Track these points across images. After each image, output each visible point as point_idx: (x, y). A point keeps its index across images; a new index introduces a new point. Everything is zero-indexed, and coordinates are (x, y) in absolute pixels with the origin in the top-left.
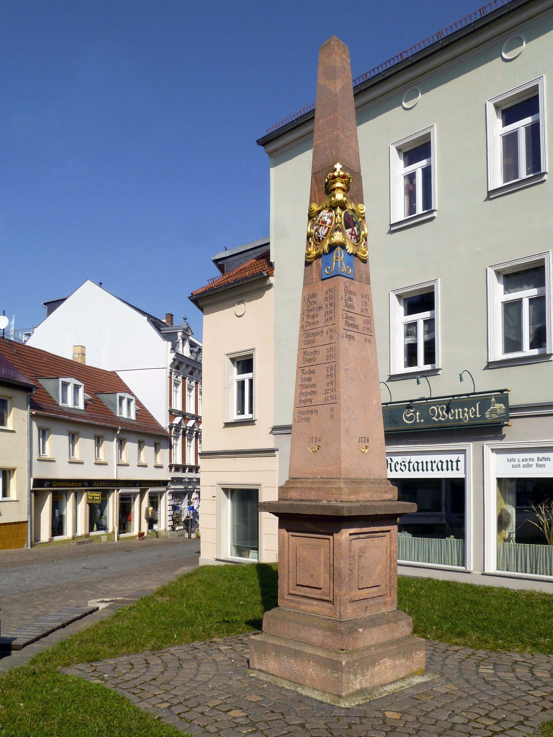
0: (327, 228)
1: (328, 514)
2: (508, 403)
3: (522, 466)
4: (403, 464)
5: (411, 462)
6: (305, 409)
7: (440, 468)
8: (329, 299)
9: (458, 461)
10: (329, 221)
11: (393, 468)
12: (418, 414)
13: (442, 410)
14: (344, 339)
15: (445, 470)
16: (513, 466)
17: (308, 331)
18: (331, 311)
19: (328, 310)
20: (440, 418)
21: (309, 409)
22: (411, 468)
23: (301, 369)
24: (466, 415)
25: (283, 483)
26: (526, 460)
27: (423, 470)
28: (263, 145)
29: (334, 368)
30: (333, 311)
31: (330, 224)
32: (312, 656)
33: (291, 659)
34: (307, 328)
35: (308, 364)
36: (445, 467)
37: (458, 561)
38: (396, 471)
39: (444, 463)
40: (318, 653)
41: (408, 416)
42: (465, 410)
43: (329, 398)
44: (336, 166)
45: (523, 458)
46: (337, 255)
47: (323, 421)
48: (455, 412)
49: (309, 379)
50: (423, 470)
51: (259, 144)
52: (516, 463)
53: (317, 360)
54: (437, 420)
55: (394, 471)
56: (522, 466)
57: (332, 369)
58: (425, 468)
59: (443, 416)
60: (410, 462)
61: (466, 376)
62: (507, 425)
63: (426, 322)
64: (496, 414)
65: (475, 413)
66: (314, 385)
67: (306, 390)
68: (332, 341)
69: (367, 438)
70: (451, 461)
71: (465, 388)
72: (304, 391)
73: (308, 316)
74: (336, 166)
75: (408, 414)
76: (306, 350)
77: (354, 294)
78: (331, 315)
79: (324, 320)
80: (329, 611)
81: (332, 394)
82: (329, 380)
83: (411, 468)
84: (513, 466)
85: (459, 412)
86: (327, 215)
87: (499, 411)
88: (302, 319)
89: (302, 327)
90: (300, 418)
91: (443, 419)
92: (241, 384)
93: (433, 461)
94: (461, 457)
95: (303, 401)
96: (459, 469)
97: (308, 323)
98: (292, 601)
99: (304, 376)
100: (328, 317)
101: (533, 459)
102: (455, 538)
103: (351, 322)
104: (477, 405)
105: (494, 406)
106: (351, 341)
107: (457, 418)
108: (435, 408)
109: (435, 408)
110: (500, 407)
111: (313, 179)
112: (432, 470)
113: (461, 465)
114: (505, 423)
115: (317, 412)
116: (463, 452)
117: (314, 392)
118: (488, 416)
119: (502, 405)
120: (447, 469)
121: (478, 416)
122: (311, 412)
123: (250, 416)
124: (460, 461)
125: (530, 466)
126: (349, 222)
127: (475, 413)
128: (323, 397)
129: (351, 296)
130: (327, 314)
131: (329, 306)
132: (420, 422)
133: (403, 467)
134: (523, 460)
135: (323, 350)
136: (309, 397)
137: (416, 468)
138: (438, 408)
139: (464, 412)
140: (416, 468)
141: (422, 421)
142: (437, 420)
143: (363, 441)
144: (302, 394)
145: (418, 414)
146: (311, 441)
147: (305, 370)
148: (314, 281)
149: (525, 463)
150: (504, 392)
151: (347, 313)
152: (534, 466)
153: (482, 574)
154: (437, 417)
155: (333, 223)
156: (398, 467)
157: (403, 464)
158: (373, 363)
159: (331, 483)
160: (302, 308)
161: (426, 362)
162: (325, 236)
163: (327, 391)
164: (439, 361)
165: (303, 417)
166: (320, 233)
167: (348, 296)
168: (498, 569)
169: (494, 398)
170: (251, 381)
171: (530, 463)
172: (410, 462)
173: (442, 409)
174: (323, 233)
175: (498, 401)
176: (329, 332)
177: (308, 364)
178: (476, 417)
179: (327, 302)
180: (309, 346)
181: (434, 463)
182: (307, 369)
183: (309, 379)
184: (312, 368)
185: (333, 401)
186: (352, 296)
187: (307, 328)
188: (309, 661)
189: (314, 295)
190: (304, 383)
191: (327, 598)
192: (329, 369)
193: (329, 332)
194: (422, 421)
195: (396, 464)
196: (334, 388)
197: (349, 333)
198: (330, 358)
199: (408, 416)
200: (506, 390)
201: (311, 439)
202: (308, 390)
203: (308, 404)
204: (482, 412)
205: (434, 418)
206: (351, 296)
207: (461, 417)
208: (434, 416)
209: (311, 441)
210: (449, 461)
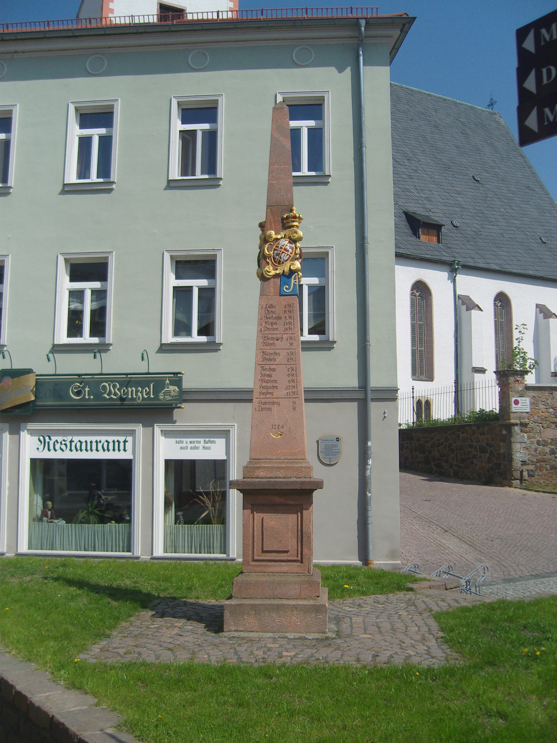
1: (307, 488)
2: (182, 387)
3: (189, 448)
4: (63, 443)
5: (73, 441)
7: (106, 448)
8: (287, 312)
9: (125, 442)
10: (290, 250)
11: (51, 447)
12: (87, 389)
13: (114, 388)
15: (111, 451)
16: (181, 448)
17: (267, 335)
20: (112, 396)
22: (73, 448)
24: (140, 394)
25: (245, 464)
26: (194, 442)
27: (86, 450)
29: (295, 369)
31: (291, 253)
32: (296, 607)
33: (273, 614)
34: (266, 332)
36: (111, 447)
37: (123, 547)
38: (55, 450)
39: (110, 444)
40: (300, 603)
43: (291, 394)
47: (285, 412)
48: (128, 391)
50: (86, 450)
52: (184, 445)
54: (108, 397)
55: (53, 451)
57: (293, 369)
58: (89, 448)
60: (71, 442)
62: (180, 408)
63: (94, 292)
64: (170, 396)
66: (275, 381)
67: (266, 384)
68: (292, 347)
70: (118, 441)
71: (142, 367)
76: (265, 350)
79: (284, 329)
81: (294, 390)
82: (290, 378)
83: (73, 448)
84: (181, 448)
85: (132, 391)
87: (173, 393)
90: (260, 408)
91: (115, 397)
93: (99, 441)
94: (130, 439)
95: (263, 393)
96: (126, 449)
97: (266, 328)
98: (259, 566)
99: (263, 372)
100: (286, 326)
102: (116, 523)
104: (152, 385)
105: (167, 388)
108: (107, 385)
109: (107, 385)
110: (173, 389)
111: (269, 211)
112: (97, 450)
113: (129, 446)
114: (179, 405)
116: (132, 433)
119: (176, 388)
120: (114, 450)
121: (152, 396)
122: (273, 403)
124: (127, 441)
125: (197, 448)
127: (148, 393)
130: (286, 324)
131: (287, 317)
133: (63, 447)
134: (191, 443)
135: (284, 353)
136: (270, 391)
137: (78, 448)
138: (109, 385)
139: (137, 391)
140: (78, 448)
141: (92, 397)
142: (108, 397)
144: (262, 387)
145: (87, 389)
146: (274, 428)
147: (264, 368)
149: (193, 445)
150: (179, 375)
152: (201, 448)
153: (152, 558)
154: (108, 395)
156: (58, 446)
157: (63, 443)
159: (297, 463)
161: (92, 334)
162: (285, 261)
164: (110, 336)
169: (169, 380)
171: (197, 445)
172: (71, 442)
173: (114, 387)
174: (285, 258)
175: (172, 383)
176: (289, 339)
178: (149, 397)
179: (286, 315)
180: (269, 347)
181: (99, 443)
183: (270, 376)
184: (273, 367)
185: (294, 396)
187: (266, 332)
188: (292, 611)
191: (295, 558)
193: (289, 339)
195: (56, 443)
196: (295, 386)
198: (290, 360)
200: (180, 373)
201: (274, 427)
203: (268, 396)
205: (106, 395)
207: (135, 397)
208: (105, 393)
209: (274, 428)
210: (116, 441)
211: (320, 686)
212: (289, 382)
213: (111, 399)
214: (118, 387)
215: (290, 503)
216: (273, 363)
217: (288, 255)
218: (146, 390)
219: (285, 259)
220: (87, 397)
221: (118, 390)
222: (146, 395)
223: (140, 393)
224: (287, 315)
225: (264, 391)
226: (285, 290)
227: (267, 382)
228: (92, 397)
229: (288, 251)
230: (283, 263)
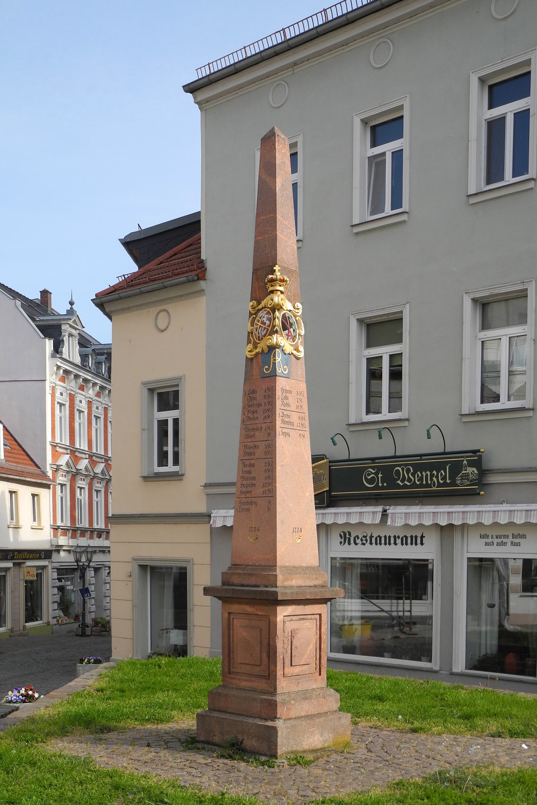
0: (266, 329)
3: (495, 544)
5: (373, 537)
6: (245, 500)
10: (268, 322)
12: (380, 475)
14: (280, 436)
16: (487, 544)
18: (269, 409)
19: (267, 407)
20: (406, 482)
21: (249, 500)
23: (242, 461)
28: (191, 92)
29: (271, 464)
30: (271, 410)
31: (269, 326)
34: (248, 423)
35: (248, 457)
41: (369, 477)
42: (434, 474)
43: (267, 492)
44: (275, 268)
45: (498, 534)
46: (274, 356)
48: (422, 475)
49: (249, 472)
51: (186, 91)
52: (489, 540)
53: (256, 455)
54: (401, 484)
56: (495, 544)
57: (269, 464)
59: (409, 480)
61: (434, 431)
64: (468, 479)
65: (444, 478)
66: (254, 478)
67: (247, 482)
69: (300, 529)
72: (244, 483)
73: (248, 411)
74: (275, 268)
75: (369, 475)
76: (246, 443)
77: (290, 392)
78: (269, 413)
80: (266, 685)
81: (269, 487)
86: (266, 316)
88: (243, 414)
89: (243, 421)
91: (408, 484)
92: (163, 424)
99: (245, 469)
100: (266, 414)
101: (508, 536)
103: (287, 420)
106: (286, 438)
107: (424, 482)
109: (400, 469)
115: (256, 503)
117: (254, 485)
118: (459, 482)
119: (475, 469)
121: (448, 481)
123: (176, 469)
125: (504, 544)
126: (286, 324)
127: (444, 478)
128: (261, 490)
129: (287, 394)
130: (265, 411)
131: (267, 404)
132: (383, 485)
134: (497, 537)
135: (262, 445)
136: (249, 489)
138: (403, 469)
139: (432, 476)
142: (401, 484)
143: (296, 531)
145: (380, 475)
148: (254, 378)
150: (478, 454)
151: (283, 411)
154: (402, 481)
155: (271, 325)
156: (359, 541)
158: (306, 457)
160: (243, 402)
163: (265, 484)
165: (243, 507)
166: (260, 333)
167: (284, 394)
168: (466, 669)
170: (176, 421)
171: (505, 540)
173: (408, 471)
175: (471, 464)
176: (267, 429)
177: (248, 457)
180: (249, 440)
182: (247, 462)
183: (249, 472)
184: (253, 462)
186: (288, 395)
187: (248, 423)
189: (254, 392)
190: (245, 475)
192: (267, 465)
194: (385, 484)
197: (285, 430)
198: (267, 454)
199: (369, 477)
200: (479, 451)
202: (248, 482)
203: (248, 495)
204: (453, 477)
205: (399, 482)
206: (287, 394)
207: (429, 482)
211: (118, 789)
212: (266, 479)
213: (405, 486)
214: (412, 471)
215: (260, 613)
216: (252, 457)
217: (265, 328)
218: (418, 476)
219: (263, 334)
220: (380, 485)
221: (413, 475)
222: (418, 481)
223: (435, 478)
224: (266, 401)
225: (244, 490)
226: (265, 371)
227: (247, 479)
228: (385, 484)
229: (265, 324)
230: (262, 339)
